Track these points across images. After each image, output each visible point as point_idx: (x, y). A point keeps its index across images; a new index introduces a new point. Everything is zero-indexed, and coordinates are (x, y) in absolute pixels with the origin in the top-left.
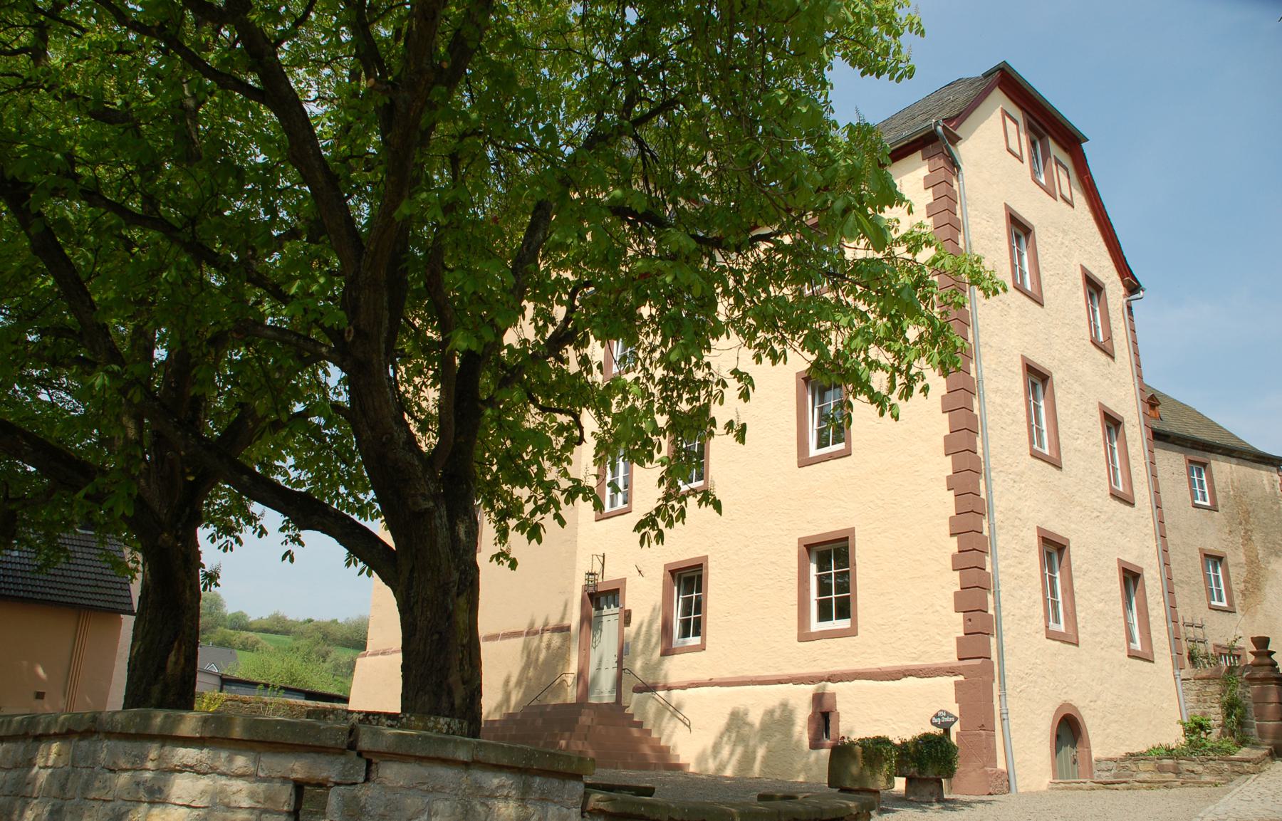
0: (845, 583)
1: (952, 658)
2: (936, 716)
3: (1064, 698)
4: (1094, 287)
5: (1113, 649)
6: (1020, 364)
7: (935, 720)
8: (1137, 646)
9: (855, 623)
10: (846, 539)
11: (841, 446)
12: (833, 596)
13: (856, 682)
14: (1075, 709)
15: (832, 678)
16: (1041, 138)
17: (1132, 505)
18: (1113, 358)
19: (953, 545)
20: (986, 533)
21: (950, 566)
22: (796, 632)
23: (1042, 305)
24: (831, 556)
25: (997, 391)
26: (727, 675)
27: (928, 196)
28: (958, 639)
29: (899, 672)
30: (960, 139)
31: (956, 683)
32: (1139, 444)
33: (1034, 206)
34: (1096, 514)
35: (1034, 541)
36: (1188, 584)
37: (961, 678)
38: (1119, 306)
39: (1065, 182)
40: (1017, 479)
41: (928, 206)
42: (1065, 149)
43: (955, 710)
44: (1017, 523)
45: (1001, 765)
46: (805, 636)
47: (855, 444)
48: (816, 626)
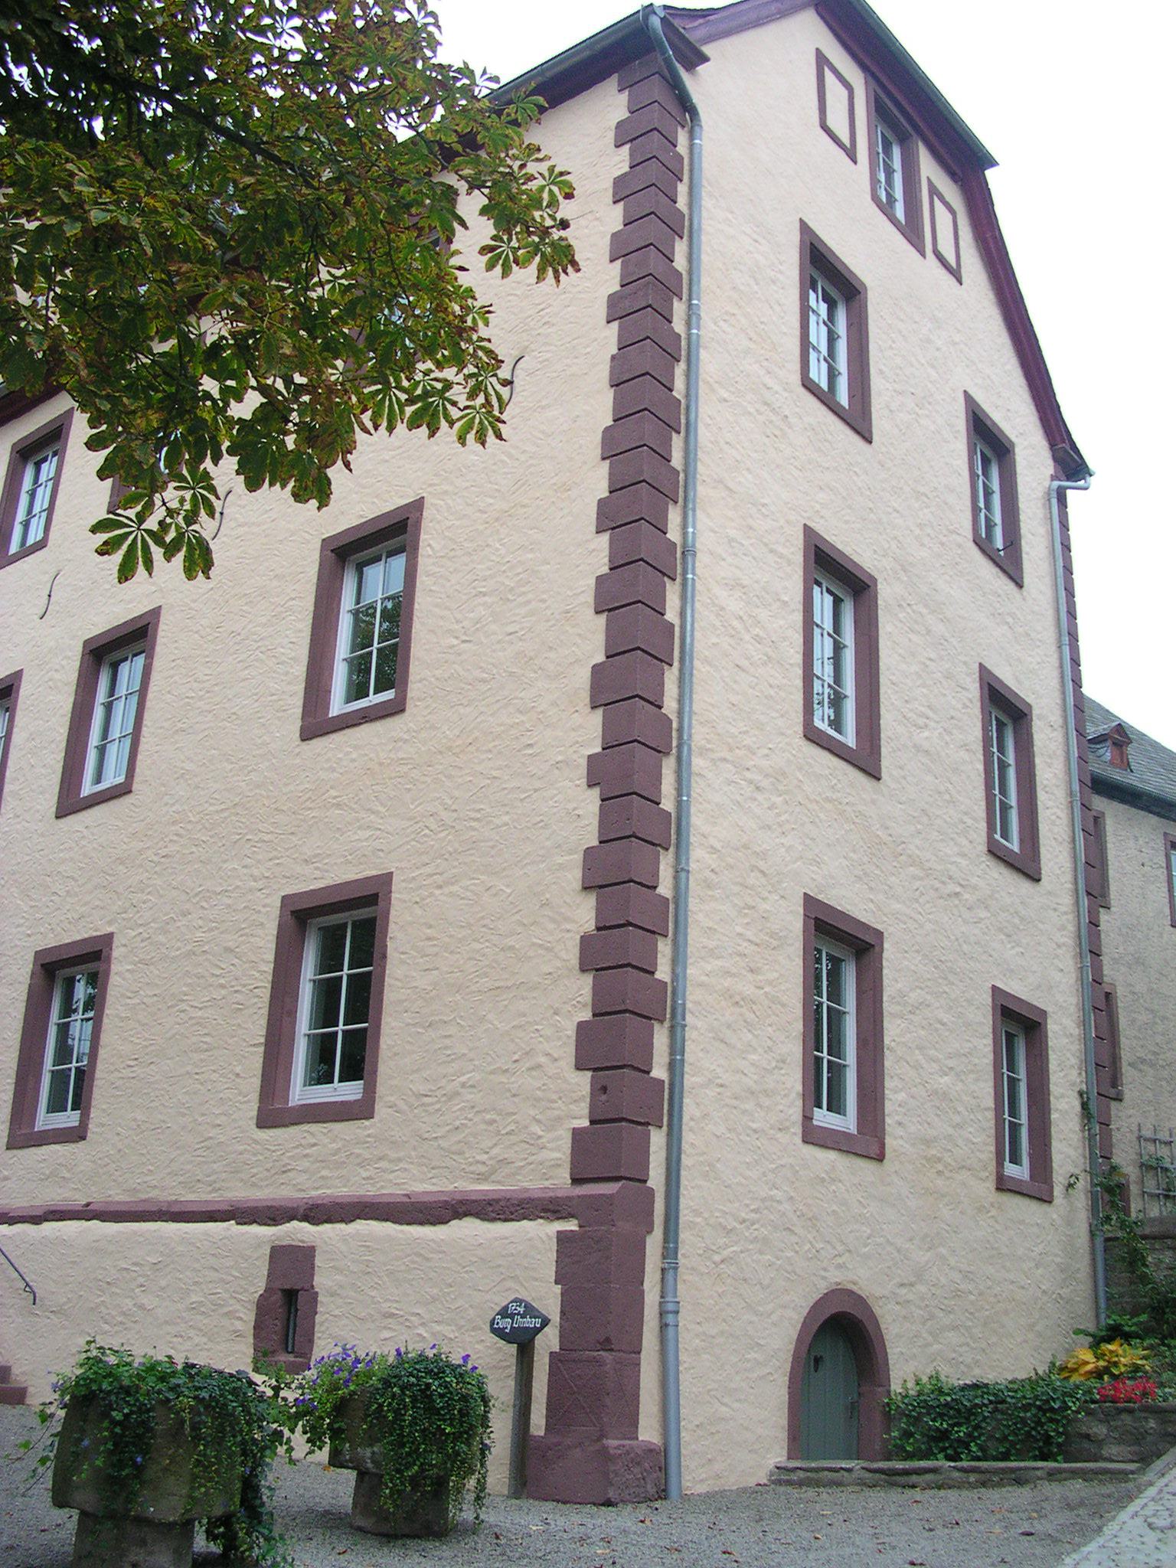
0: (364, 998)
1: (560, 1180)
2: (504, 1313)
3: (835, 1277)
4: (988, 442)
5: (964, 1175)
6: (799, 542)
7: (506, 1324)
8: (1018, 1172)
9: (370, 1092)
10: (372, 900)
11: (389, 695)
12: (341, 1027)
13: (360, 1226)
14: (860, 1301)
15: (317, 1213)
16: (903, 140)
17: (1036, 879)
18: (1020, 586)
19: (584, 914)
20: (665, 889)
21: (575, 962)
22: (255, 1106)
23: (869, 440)
24: (340, 936)
25: (735, 585)
26: (117, 1195)
27: (620, 162)
28: (577, 1133)
29: (446, 1205)
30: (705, 59)
31: (562, 1238)
32: (1059, 765)
33: (866, 245)
34: (952, 888)
35: (796, 925)
36: (1152, 1065)
37: (572, 1225)
38: (1040, 492)
39: (946, 222)
40: (765, 783)
41: (618, 182)
42: (953, 175)
43: (549, 1299)
44: (753, 879)
45: (648, 1432)
46: (273, 1113)
47: (414, 689)
48: (300, 1092)
